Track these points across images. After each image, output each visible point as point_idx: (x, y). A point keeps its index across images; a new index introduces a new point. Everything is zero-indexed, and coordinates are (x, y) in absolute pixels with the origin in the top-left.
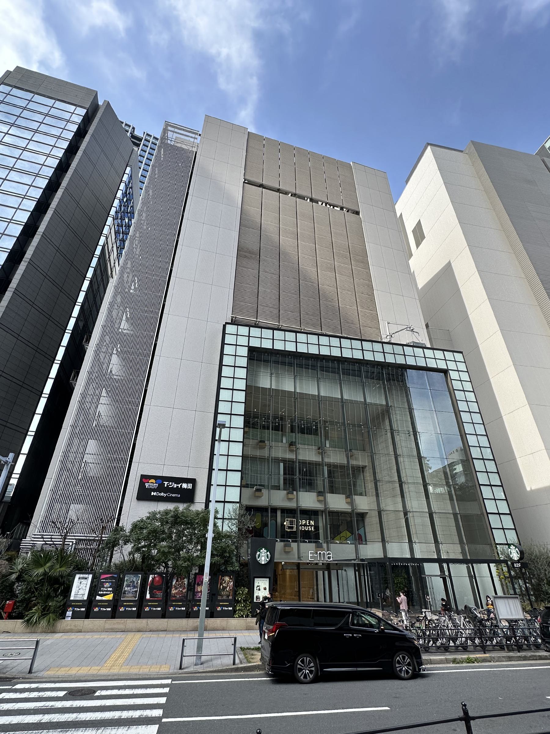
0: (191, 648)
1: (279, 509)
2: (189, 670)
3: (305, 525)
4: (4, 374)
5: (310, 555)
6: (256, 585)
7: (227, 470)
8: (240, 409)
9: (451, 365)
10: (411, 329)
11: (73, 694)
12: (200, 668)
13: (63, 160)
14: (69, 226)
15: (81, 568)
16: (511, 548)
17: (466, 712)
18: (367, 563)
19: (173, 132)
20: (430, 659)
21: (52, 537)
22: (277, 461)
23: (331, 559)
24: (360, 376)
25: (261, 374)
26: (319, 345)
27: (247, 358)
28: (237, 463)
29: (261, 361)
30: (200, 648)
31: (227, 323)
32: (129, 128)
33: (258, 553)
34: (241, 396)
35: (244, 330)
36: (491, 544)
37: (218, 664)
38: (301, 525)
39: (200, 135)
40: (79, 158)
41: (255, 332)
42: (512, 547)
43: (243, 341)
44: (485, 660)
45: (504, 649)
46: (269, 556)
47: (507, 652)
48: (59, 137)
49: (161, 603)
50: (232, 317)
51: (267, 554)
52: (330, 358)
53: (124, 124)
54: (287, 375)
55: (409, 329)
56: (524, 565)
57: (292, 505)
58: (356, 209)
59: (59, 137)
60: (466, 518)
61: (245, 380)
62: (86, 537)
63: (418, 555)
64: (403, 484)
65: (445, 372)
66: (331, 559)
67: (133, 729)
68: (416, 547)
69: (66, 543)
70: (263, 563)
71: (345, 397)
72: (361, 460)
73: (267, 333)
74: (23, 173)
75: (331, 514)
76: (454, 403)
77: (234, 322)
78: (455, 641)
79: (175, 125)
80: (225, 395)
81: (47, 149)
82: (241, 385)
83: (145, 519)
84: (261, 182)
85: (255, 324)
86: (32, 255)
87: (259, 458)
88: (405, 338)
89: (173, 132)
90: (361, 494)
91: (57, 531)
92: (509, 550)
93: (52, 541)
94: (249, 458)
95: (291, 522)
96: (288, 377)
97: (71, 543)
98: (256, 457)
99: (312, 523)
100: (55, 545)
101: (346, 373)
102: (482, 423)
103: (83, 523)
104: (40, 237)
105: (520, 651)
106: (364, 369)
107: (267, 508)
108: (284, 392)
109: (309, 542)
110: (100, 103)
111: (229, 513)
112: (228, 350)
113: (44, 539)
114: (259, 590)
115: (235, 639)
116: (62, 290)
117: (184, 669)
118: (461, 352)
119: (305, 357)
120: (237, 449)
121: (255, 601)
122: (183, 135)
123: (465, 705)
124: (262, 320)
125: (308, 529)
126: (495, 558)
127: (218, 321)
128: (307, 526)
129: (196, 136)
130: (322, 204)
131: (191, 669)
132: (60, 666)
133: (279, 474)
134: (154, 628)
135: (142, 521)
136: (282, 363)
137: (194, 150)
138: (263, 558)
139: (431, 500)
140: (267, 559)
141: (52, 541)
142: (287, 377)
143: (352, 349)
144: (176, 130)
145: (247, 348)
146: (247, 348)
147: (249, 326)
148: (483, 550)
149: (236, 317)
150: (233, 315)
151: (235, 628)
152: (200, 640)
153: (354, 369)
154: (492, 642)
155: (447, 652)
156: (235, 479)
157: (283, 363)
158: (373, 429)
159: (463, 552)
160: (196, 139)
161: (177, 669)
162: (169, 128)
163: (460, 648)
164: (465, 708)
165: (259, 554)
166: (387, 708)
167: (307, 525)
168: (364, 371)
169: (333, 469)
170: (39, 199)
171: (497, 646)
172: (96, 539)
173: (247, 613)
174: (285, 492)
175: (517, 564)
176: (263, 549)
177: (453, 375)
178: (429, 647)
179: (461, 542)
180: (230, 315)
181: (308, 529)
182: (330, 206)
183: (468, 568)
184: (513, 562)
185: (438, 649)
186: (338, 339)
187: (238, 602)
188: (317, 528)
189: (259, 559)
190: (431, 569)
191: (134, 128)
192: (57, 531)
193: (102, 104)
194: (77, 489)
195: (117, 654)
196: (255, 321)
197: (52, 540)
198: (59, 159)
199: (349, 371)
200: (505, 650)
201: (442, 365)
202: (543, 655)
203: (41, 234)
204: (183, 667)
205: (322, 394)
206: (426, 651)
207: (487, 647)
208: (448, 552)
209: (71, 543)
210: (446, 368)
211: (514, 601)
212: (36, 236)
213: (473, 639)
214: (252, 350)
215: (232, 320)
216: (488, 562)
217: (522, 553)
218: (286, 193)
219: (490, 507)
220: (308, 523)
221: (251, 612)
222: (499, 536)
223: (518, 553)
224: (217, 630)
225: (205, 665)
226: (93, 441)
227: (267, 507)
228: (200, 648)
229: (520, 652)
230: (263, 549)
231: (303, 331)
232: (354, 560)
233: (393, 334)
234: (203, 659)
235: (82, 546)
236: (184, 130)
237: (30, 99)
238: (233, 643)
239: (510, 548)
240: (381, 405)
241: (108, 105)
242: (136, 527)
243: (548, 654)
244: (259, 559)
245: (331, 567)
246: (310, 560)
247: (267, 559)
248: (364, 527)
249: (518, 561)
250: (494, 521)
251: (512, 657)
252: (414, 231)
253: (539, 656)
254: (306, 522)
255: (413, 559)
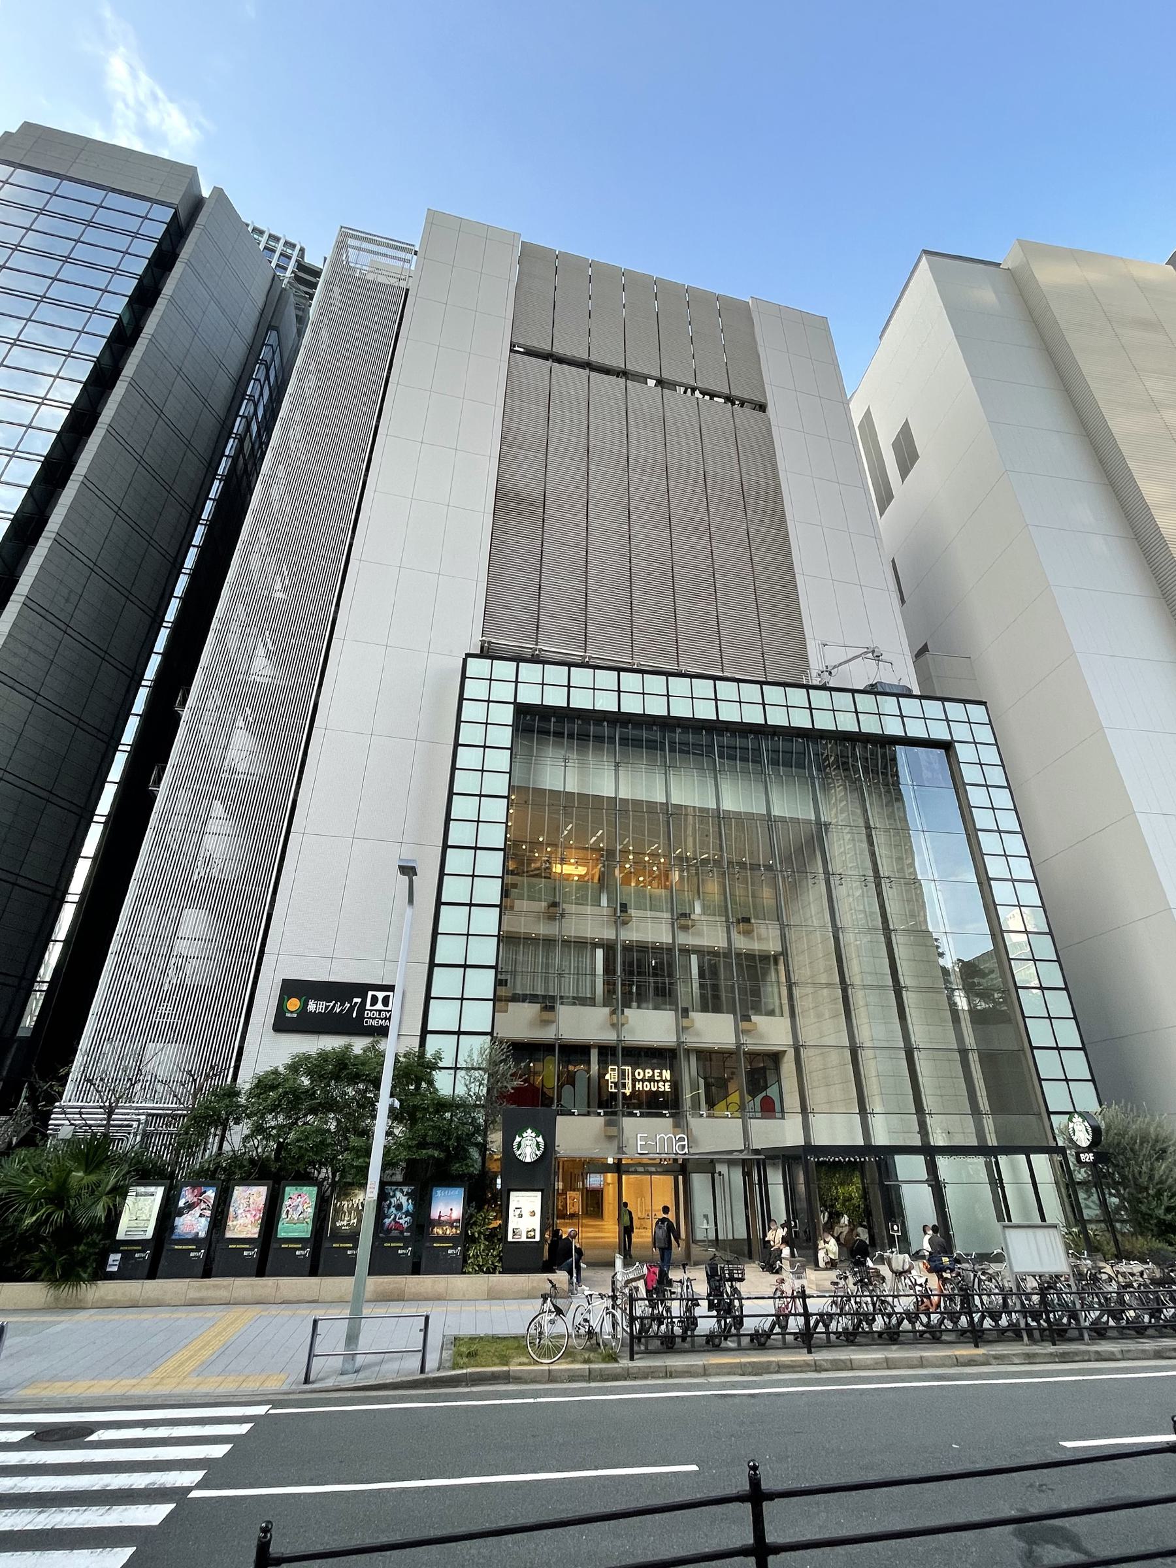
0: (332, 1337)
1: (594, 1046)
2: (324, 1385)
3: (651, 1080)
4: (7, 777)
5: (639, 1143)
6: (513, 1205)
7: (465, 966)
8: (495, 836)
9: (960, 732)
10: (875, 655)
11: (46, 1437)
12: (348, 1381)
13: (125, 321)
14: (142, 462)
15: (146, 1173)
16: (1074, 1120)
17: (755, 1482)
18: (764, 1157)
19: (359, 249)
20: (851, 1360)
21: (82, 1110)
22: (583, 945)
23: (686, 1150)
24: (757, 761)
25: (548, 763)
26: (692, 698)
27: (511, 728)
28: (485, 952)
29: (548, 733)
30: (352, 1338)
31: (468, 655)
32: (293, 251)
33: (518, 1139)
34: (497, 810)
35: (505, 669)
36: (1040, 1114)
37: (392, 1371)
38: (643, 1080)
39: (416, 253)
40: (160, 313)
41: (530, 671)
42: (1077, 1119)
43: (504, 692)
44: (974, 1361)
45: (1020, 1338)
46: (542, 1146)
47: (1027, 1345)
48: (115, 271)
49: (428, 1244)
50: (483, 642)
51: (537, 1142)
52: (690, 723)
53: (282, 242)
54: (606, 763)
55: (870, 655)
56: (1101, 1157)
57: (546, 1034)
58: (757, 397)
59: (115, 271)
60: (989, 1059)
61: (508, 775)
62: (168, 1109)
63: (881, 1139)
64: (904, 992)
65: (947, 746)
66: (686, 1150)
67: (117, 1511)
68: (816, 1121)
69: (112, 1122)
70: (528, 1160)
71: (777, 812)
72: (766, 940)
73: (556, 674)
74: (46, 347)
75: (748, 1056)
76: (965, 810)
77: (487, 653)
78: (1038, 1318)
79: (391, 242)
80: (463, 808)
81: (90, 298)
82: (499, 785)
83: (281, 1069)
84: (585, 356)
85: (533, 655)
86: (62, 524)
87: (574, 942)
88: (861, 674)
89: (359, 249)
90: (771, 1013)
91: (173, 1099)
92: (1071, 1125)
93: (83, 1119)
94: (572, 944)
95: (622, 1074)
96: (552, 763)
97: (135, 1124)
98: (518, 936)
99: (667, 1074)
100: (90, 1126)
101: (729, 754)
102: (1026, 855)
103: (116, 1080)
104: (77, 485)
105: (1057, 1342)
106: (767, 746)
107: (615, 1047)
108: (599, 799)
109: (642, 1115)
110: (206, 193)
111: (469, 1056)
112: (471, 711)
113: (67, 1116)
114: (521, 1216)
115: (427, 1318)
116: (131, 597)
117: (313, 1382)
118: (984, 703)
119: (608, 722)
120: (488, 921)
121: (510, 1239)
122: (386, 255)
123: (755, 1468)
124: (547, 647)
125: (658, 1087)
126: (1048, 1143)
127: (451, 651)
128: (654, 1081)
129: (409, 256)
130: (685, 392)
131: (329, 1383)
132: (54, 1379)
133: (594, 974)
134: (291, 1296)
135: (276, 1072)
136: (635, 742)
137: (403, 284)
138: (528, 1151)
139: (909, 1021)
140: (538, 1153)
141: (83, 1119)
142: (606, 767)
143: (740, 702)
144: (365, 245)
145: (512, 706)
146: (512, 706)
147: (518, 659)
148: (1023, 1127)
149: (489, 643)
150: (484, 638)
151: (464, 1295)
152: (355, 1322)
153: (746, 746)
154: (996, 1322)
155: (894, 1344)
156: (483, 983)
157: (637, 743)
158: (785, 873)
159: (980, 1132)
160: (409, 262)
161: (298, 1383)
162: (351, 242)
163: (968, 1334)
164: (756, 1474)
165: (520, 1142)
166: (694, 1468)
167: (659, 1080)
168: (767, 751)
169: (712, 962)
170: (73, 405)
171: (1128, 1328)
172: (177, 1115)
173: (493, 1263)
174: (607, 1010)
175: (1086, 1154)
176: (529, 1131)
177: (964, 753)
178: (983, 1331)
179: (976, 1111)
180: (478, 638)
181: (658, 1087)
182: (703, 393)
183: (988, 1166)
184: (1079, 1150)
185: (962, 1335)
186: (712, 682)
187: (473, 1240)
188: (676, 1084)
189: (519, 1152)
190: (909, 1167)
191: (302, 250)
192: (173, 1099)
193: (207, 197)
194: (167, 1012)
195: (186, 1353)
196: (531, 648)
197: (83, 1116)
198: (115, 318)
199: (746, 751)
200: (1023, 1340)
201: (939, 732)
202: (1107, 1351)
203: (81, 478)
204: (311, 1379)
205: (675, 800)
206: (934, 1338)
207: (1108, 1330)
208: (949, 1133)
209: (135, 1124)
210: (904, 734)
211: (1047, 1235)
212: (69, 484)
213: (996, 1316)
214: (523, 712)
215: (482, 648)
216: (1027, 1151)
217: (1096, 1131)
218: (643, 379)
219: (1039, 1033)
220: (656, 1074)
221: (500, 1260)
222: (1056, 1096)
223: (1088, 1132)
224: (426, 1300)
225: (361, 1375)
226: (195, 912)
227: (615, 1045)
228: (352, 1338)
229: (1055, 1345)
230: (529, 1131)
231: (636, 667)
232: (741, 1151)
233: (835, 667)
234: (360, 1360)
235: (152, 1129)
236: (388, 245)
237: (98, 203)
238: (423, 1327)
239: (1072, 1122)
240: (809, 822)
241: (218, 193)
242: (264, 1085)
243: (1116, 1349)
244: (519, 1152)
245: (689, 1167)
246: (639, 1152)
247: (538, 1153)
248: (779, 1081)
249: (1088, 1149)
250: (1047, 1064)
251: (1035, 1355)
252: (896, 446)
253: (1097, 1352)
254: (654, 1073)
255: (868, 1149)
